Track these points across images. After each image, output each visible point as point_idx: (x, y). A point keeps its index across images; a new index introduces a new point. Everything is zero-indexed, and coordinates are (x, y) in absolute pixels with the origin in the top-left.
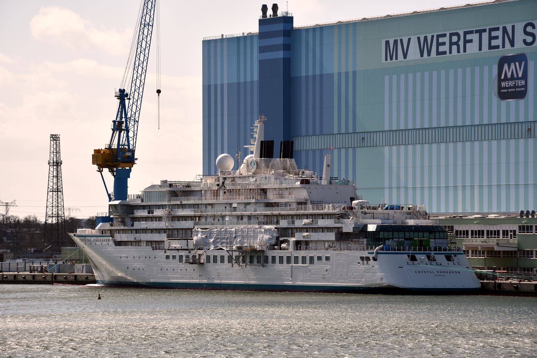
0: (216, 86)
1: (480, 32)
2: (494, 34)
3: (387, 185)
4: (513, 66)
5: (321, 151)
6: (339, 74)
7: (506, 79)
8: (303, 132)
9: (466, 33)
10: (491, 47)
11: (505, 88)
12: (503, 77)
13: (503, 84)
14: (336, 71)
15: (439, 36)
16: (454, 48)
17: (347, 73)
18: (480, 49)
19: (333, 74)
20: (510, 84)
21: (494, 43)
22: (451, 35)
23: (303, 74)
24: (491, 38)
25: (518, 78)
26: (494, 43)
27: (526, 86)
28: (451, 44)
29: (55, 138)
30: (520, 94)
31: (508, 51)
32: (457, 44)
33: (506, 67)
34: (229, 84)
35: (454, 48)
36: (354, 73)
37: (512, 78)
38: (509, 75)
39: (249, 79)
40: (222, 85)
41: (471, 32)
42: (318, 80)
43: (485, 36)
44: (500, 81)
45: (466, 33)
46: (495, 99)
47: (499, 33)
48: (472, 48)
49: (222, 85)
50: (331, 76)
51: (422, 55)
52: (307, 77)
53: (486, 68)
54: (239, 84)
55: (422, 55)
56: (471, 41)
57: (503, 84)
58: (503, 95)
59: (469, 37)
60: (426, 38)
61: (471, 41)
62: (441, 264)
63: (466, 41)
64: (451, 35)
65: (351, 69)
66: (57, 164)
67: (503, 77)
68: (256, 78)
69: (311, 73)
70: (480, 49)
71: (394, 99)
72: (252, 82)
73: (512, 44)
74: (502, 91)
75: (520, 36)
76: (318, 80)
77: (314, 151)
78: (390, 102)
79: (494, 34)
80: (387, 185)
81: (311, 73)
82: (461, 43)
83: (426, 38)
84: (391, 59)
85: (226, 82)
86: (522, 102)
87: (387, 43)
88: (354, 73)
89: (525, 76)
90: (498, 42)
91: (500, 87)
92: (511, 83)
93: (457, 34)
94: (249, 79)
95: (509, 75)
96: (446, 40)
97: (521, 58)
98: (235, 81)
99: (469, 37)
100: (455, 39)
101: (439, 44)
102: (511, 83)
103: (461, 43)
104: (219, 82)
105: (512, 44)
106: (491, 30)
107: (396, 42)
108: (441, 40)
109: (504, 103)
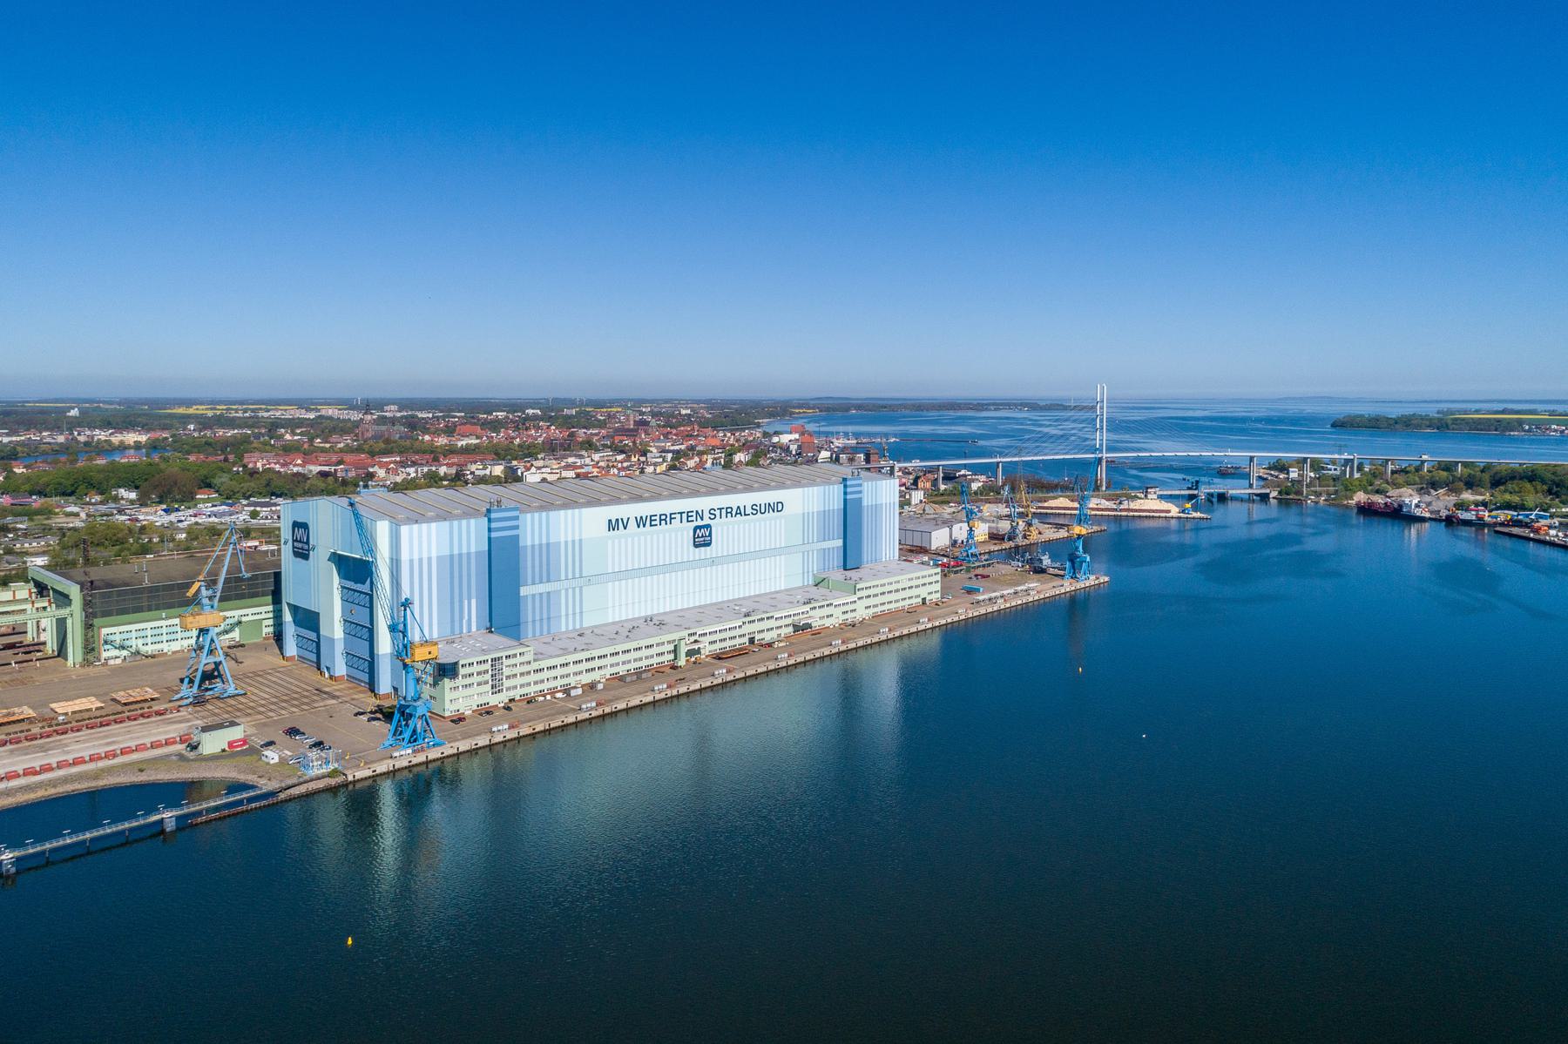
0: (421, 560)
1: (681, 513)
2: (690, 514)
3: (610, 604)
4: (702, 530)
5: (549, 593)
6: (566, 542)
8: (530, 581)
16: (663, 522)
17: (573, 541)
18: (681, 522)
19: (560, 543)
21: (653, 523)
22: (660, 515)
23: (866, 504)
24: (688, 516)
28: (661, 520)
31: (700, 523)
32: (665, 520)
33: (698, 531)
34: (439, 558)
35: (663, 522)
36: (580, 540)
37: (702, 536)
39: (831, 508)
40: (430, 559)
42: (537, 548)
43: (685, 516)
45: (671, 514)
46: (692, 548)
47: (694, 514)
48: (676, 522)
49: (430, 559)
51: (639, 527)
53: (685, 533)
54: (452, 556)
55: (639, 527)
58: (696, 546)
59: (673, 516)
60: (641, 517)
62: (861, 579)
63: (671, 519)
64: (660, 515)
65: (577, 538)
69: (464, 551)
70: (681, 522)
71: (537, 569)
76: (537, 548)
77: (829, 549)
78: (469, 575)
79: (690, 514)
80: (610, 604)
81: (464, 551)
82: (668, 519)
83: (641, 517)
84: (614, 529)
85: (434, 555)
87: (610, 521)
88: (580, 540)
89: (710, 535)
90: (694, 518)
92: (702, 539)
93: (731, 508)
94: (537, 542)
96: (658, 518)
97: (708, 526)
98: (447, 553)
99: (673, 516)
101: (651, 520)
103: (668, 519)
104: (425, 556)
107: (617, 520)
109: (697, 549)
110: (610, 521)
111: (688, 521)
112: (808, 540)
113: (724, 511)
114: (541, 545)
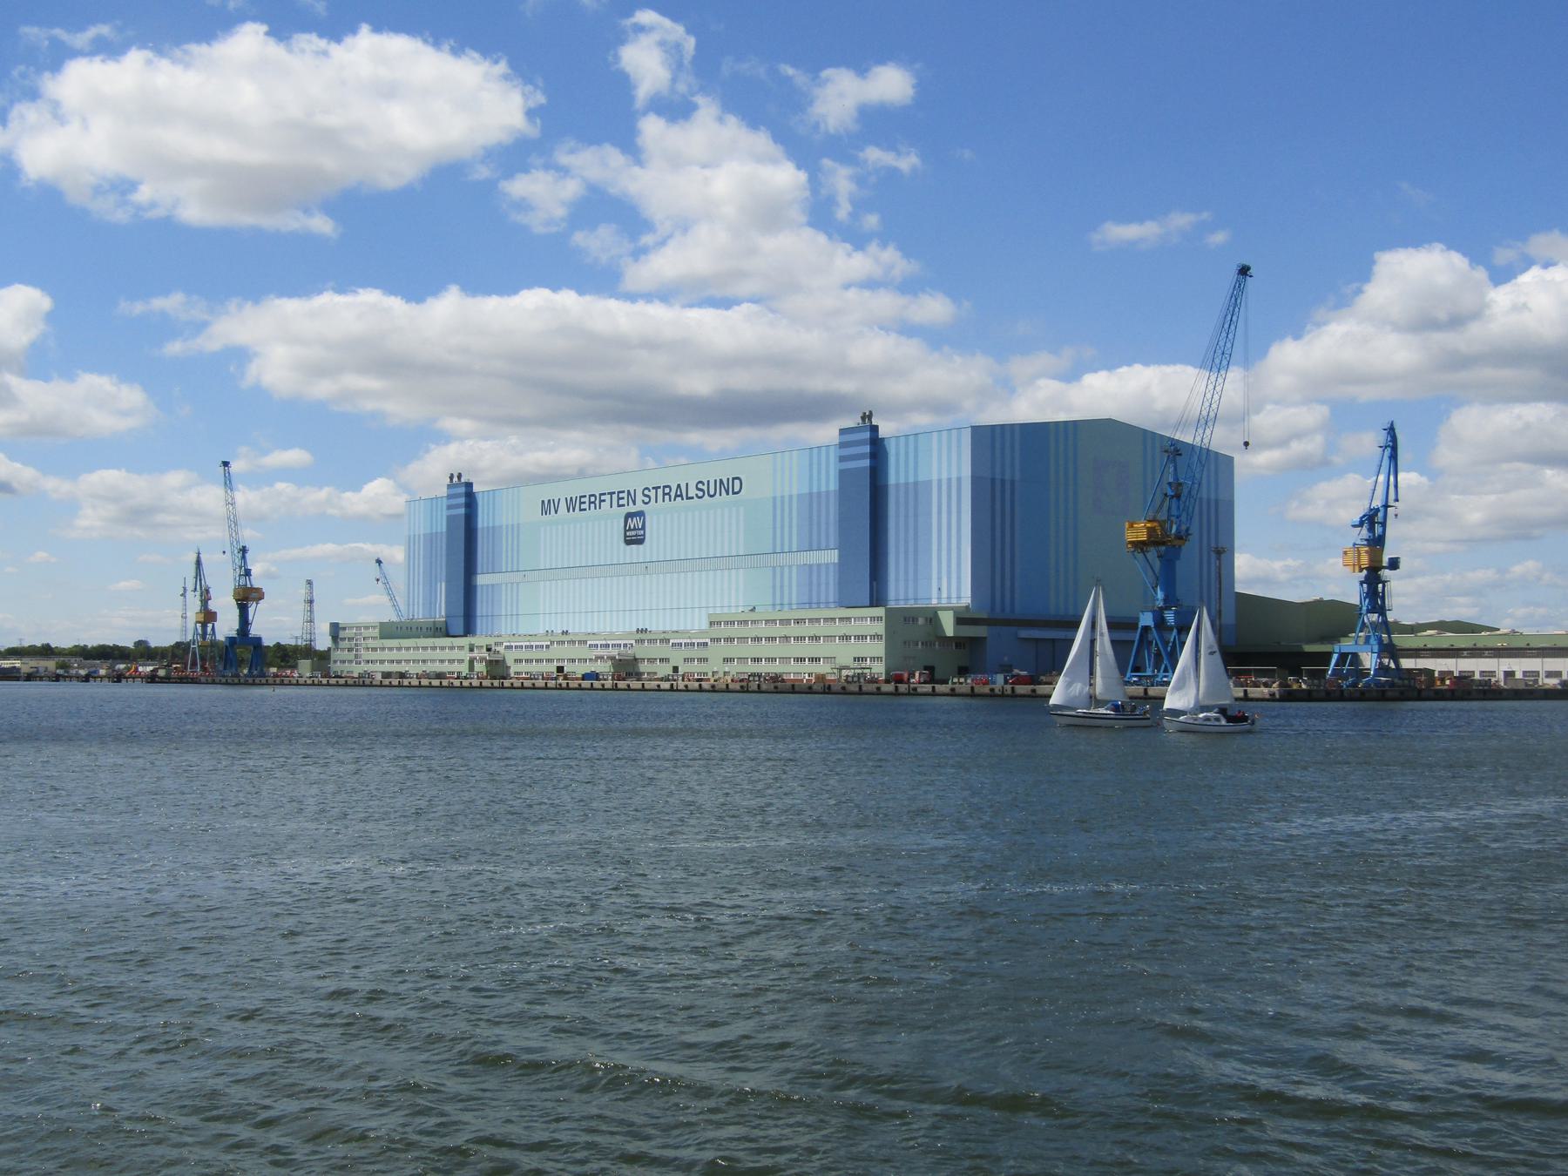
1: (611, 494)
5: (493, 585)
6: (940, 481)
7: (630, 530)
9: (601, 495)
10: (619, 506)
14: (935, 477)
15: (581, 497)
24: (619, 499)
25: (639, 529)
26: (621, 502)
27: (644, 535)
28: (590, 503)
29: (310, 583)
30: (640, 541)
31: (632, 509)
32: (668, 494)
35: (592, 505)
37: (635, 529)
38: (632, 527)
41: (604, 494)
43: (615, 496)
44: (626, 531)
46: (622, 544)
47: (625, 495)
48: (605, 505)
50: (501, 527)
52: (897, 485)
54: (811, 494)
56: (604, 501)
58: (629, 542)
59: (603, 497)
61: (604, 501)
64: (590, 496)
65: (515, 523)
66: (311, 602)
68: (444, 530)
69: (491, 525)
72: (828, 492)
73: (634, 503)
75: (639, 497)
79: (621, 495)
82: (597, 502)
85: (422, 533)
86: (641, 546)
87: (543, 502)
89: (643, 528)
91: (626, 536)
92: (633, 533)
95: (632, 527)
96: (586, 500)
97: (640, 514)
98: (806, 491)
99: (603, 497)
100: (593, 499)
101: (581, 503)
102: (633, 533)
103: (597, 502)
105: (634, 503)
106: (619, 492)
107: (549, 501)
108: (583, 500)
110: (543, 502)
111: (619, 506)
112: (790, 546)
113: (615, 496)
114: (513, 525)
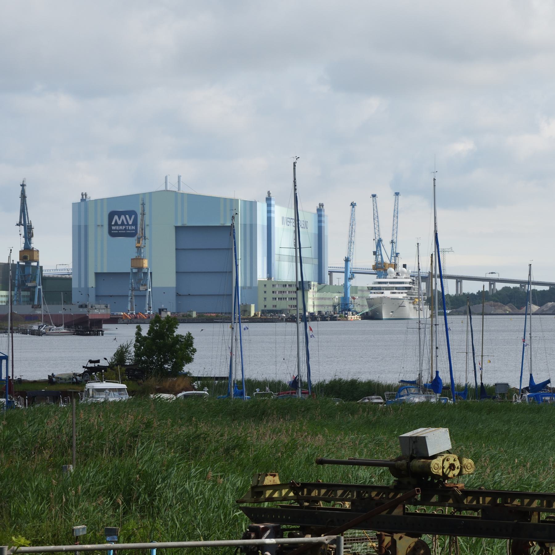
11: (116, 230)
12: (113, 223)
13: (113, 228)
20: (120, 228)
33: (116, 217)
44: (110, 225)
57: (113, 228)
67: (113, 223)
74: (112, 232)
